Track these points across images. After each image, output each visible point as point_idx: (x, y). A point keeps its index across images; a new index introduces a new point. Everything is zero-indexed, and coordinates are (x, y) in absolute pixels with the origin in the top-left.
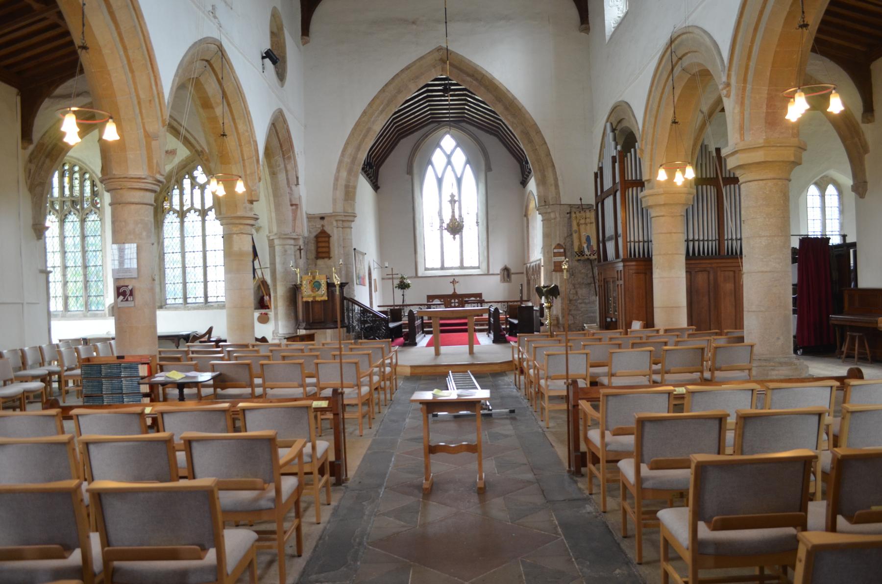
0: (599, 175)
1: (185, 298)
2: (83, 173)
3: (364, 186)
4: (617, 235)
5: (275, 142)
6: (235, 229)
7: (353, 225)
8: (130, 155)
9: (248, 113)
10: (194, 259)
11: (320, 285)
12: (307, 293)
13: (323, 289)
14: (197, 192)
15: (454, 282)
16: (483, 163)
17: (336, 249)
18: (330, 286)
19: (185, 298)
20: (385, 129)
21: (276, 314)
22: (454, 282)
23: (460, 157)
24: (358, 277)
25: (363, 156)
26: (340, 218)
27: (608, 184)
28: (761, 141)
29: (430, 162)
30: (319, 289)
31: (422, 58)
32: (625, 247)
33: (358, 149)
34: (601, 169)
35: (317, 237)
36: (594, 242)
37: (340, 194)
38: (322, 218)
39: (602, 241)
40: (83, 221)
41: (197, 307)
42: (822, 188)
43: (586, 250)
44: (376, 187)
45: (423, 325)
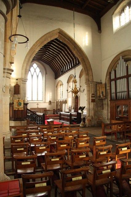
7: (26, 83)
11: (21, 104)
12: (16, 107)
15: (38, 104)
17: (21, 91)
22: (38, 104)
23: (38, 70)
26: (23, 80)
30: (20, 106)
31: (54, 31)
33: (30, 57)
36: (104, 93)
37: (24, 71)
43: (101, 96)
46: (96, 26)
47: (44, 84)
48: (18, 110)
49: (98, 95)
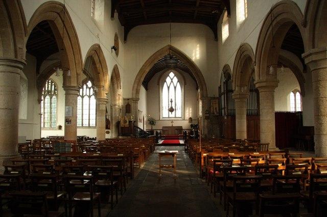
0: (220, 88)
1: (82, 124)
2: (52, 82)
3: (143, 91)
4: (225, 108)
5: (114, 75)
6: (100, 103)
8: (72, 80)
9: (107, 66)
10: (86, 112)
13: (128, 123)
14: (88, 90)
15: (172, 122)
16: (183, 82)
17: (133, 110)
18: (130, 122)
19: (82, 124)
20: (150, 70)
21: (112, 131)
22: (172, 122)
23: (175, 80)
24: (140, 120)
25: (142, 79)
27: (222, 91)
28: (265, 80)
29: (165, 81)
32: (227, 111)
34: (220, 86)
35: (126, 106)
37: (135, 92)
38: (128, 100)
39: (220, 109)
40: (51, 98)
41: (86, 127)
42: (295, 92)
44: (146, 89)
45: (161, 137)
46: (212, 35)
47: (183, 99)
48: (124, 127)
49: (212, 112)
